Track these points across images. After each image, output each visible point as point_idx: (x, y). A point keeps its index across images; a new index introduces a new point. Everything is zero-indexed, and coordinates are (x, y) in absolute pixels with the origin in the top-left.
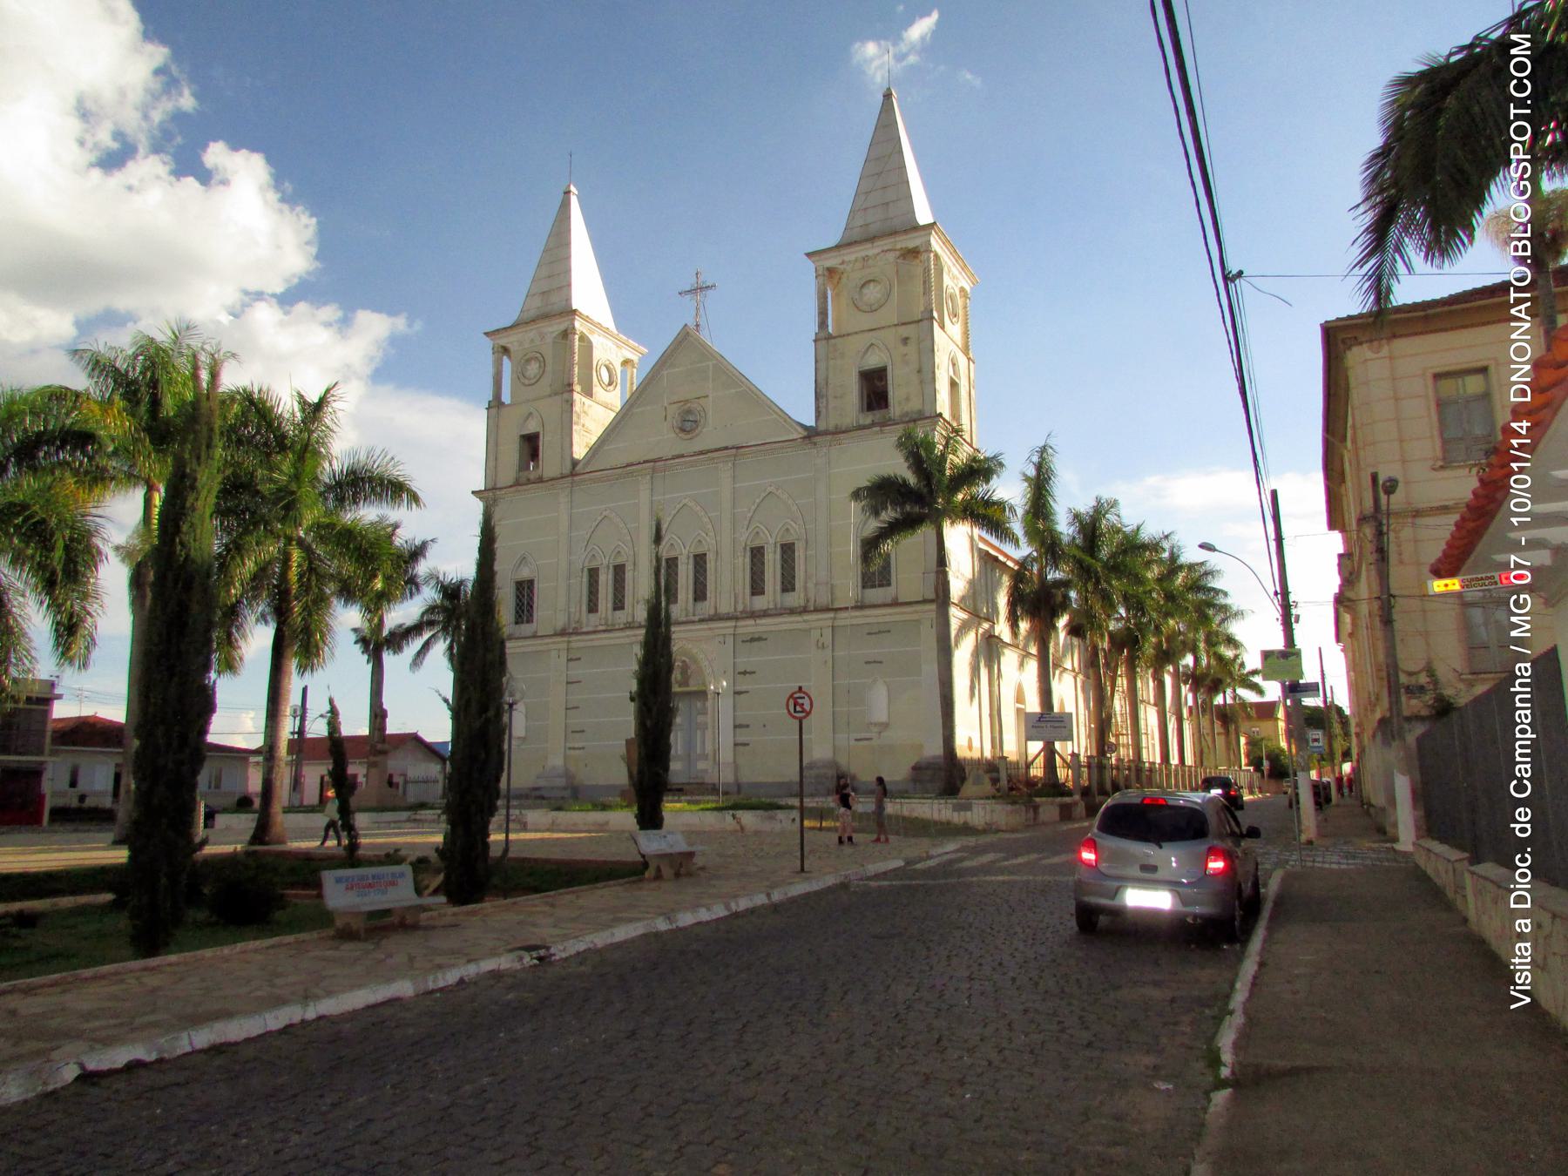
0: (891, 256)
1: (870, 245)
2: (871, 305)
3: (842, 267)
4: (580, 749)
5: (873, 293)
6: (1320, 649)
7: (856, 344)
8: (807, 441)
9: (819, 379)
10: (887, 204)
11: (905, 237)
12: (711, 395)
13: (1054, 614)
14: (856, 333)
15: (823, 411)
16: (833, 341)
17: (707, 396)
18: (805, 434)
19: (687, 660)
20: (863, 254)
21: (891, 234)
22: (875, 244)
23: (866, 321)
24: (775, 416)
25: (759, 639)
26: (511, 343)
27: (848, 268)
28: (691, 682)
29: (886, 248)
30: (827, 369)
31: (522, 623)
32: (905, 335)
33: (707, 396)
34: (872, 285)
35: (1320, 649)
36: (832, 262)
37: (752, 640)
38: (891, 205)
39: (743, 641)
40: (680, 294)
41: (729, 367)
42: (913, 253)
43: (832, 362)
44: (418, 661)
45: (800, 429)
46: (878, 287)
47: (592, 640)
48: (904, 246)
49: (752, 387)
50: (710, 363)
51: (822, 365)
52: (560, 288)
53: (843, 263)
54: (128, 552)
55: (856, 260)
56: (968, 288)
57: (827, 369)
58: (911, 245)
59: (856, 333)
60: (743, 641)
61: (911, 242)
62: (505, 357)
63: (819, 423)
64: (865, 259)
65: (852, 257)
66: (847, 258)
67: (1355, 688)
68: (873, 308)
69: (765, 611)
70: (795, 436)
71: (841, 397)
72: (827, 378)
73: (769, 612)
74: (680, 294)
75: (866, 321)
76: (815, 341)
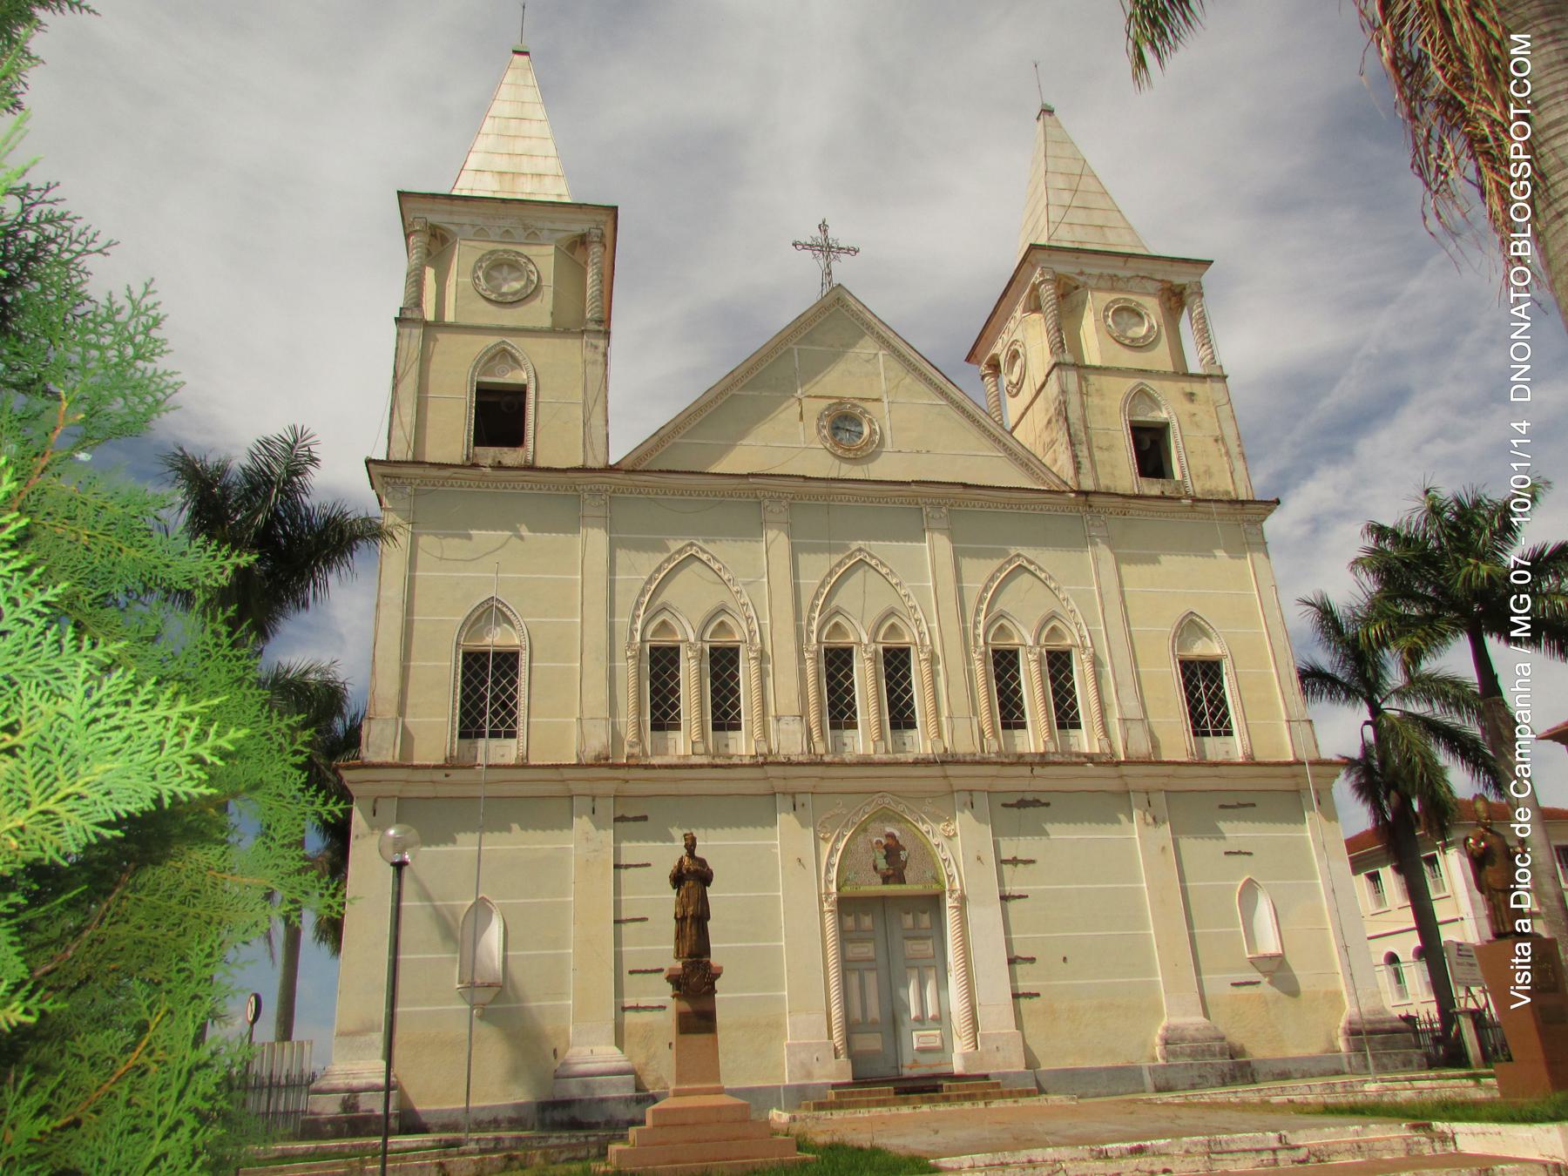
4: (651, 1008)
19: (897, 834)
20: (1111, 272)
23: (1128, 359)
25: (1036, 803)
28: (909, 874)
31: (481, 735)
37: (1022, 804)
39: (1005, 805)
40: (795, 245)
44: (690, 842)
47: (676, 780)
53: (1081, 273)
54: (481, 1017)
56: (154, 680)
60: (1005, 805)
65: (1096, 271)
67: (1422, 871)
69: (1043, 755)
73: (1051, 758)
75: (1128, 359)
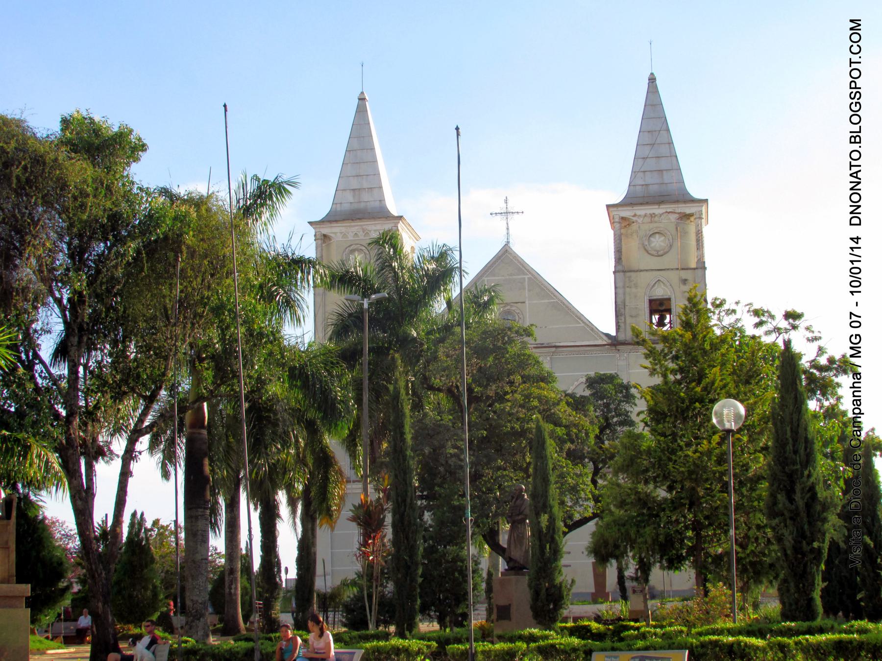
0: (673, 217)
1: (657, 207)
2: (658, 251)
3: (634, 219)
5: (658, 242)
6: (652, 80)
7: (644, 279)
8: (614, 348)
9: (618, 300)
10: (662, 171)
11: (684, 205)
12: (527, 302)
13: (665, 555)
14: (647, 270)
15: (622, 325)
16: (628, 274)
17: (524, 302)
18: (610, 341)
20: (651, 212)
21: (674, 202)
22: (661, 207)
24: (583, 325)
26: (335, 233)
27: (640, 220)
29: (668, 211)
30: (624, 294)
32: (684, 277)
33: (524, 302)
34: (657, 236)
35: (652, 80)
36: (627, 213)
38: (665, 173)
40: (491, 214)
41: (544, 283)
42: (686, 217)
43: (628, 290)
45: (605, 338)
46: (663, 238)
48: (682, 211)
49: (564, 301)
50: (526, 277)
51: (620, 291)
52: (371, 189)
53: (635, 215)
55: (645, 215)
57: (624, 294)
58: (688, 211)
59: (647, 270)
61: (688, 209)
62: (613, 333)
63: (619, 333)
64: (652, 216)
66: (638, 213)
68: (660, 253)
70: (600, 342)
71: (635, 317)
72: (624, 300)
74: (491, 214)
76: (614, 272)
